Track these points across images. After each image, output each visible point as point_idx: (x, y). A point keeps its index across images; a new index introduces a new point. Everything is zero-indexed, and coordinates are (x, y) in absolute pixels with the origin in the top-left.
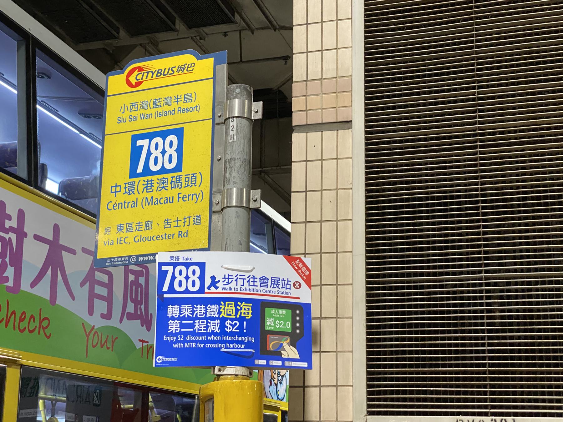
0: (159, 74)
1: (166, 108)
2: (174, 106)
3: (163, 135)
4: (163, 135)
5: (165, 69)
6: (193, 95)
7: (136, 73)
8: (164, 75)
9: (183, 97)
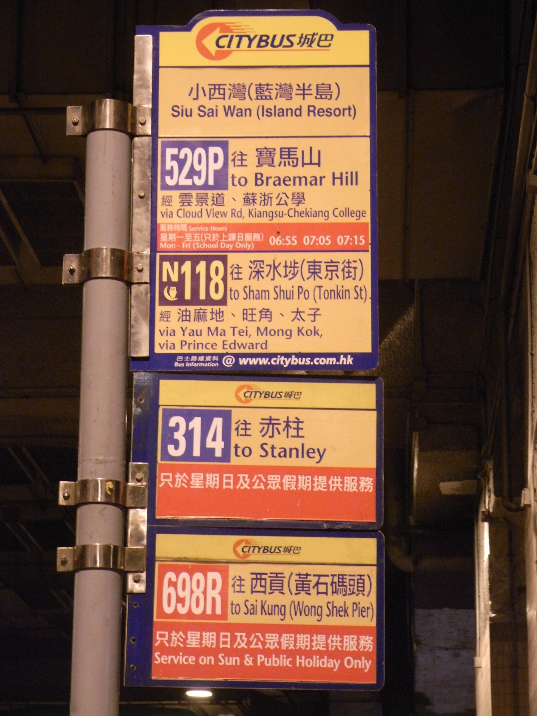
0: (263, 44)
1: (282, 103)
2: (296, 102)
3: (206, 144)
4: (206, 144)
5: (275, 37)
6: (334, 89)
7: (217, 34)
8: (272, 45)
9: (314, 88)
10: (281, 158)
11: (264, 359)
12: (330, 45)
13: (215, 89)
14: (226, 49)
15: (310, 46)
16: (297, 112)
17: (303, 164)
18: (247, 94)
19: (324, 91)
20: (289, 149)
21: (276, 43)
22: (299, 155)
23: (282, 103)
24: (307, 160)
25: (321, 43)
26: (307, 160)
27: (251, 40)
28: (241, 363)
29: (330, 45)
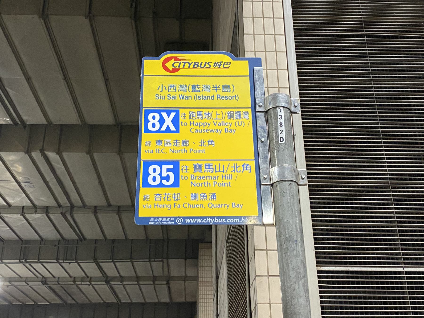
0: (196, 66)
1: (205, 94)
2: (213, 93)
5: (202, 63)
6: (231, 87)
7: (172, 61)
8: (200, 67)
9: (221, 87)
10: (205, 168)
11: (199, 220)
12: (229, 67)
13: (171, 87)
14: (177, 68)
15: (219, 67)
16: (212, 98)
17: (216, 171)
18: (187, 90)
19: (226, 88)
20: (209, 164)
21: (203, 66)
22: (214, 167)
23: (205, 94)
24: (218, 170)
25: (225, 66)
26: (218, 170)
27: (190, 65)
28: (186, 222)
29: (229, 67)
